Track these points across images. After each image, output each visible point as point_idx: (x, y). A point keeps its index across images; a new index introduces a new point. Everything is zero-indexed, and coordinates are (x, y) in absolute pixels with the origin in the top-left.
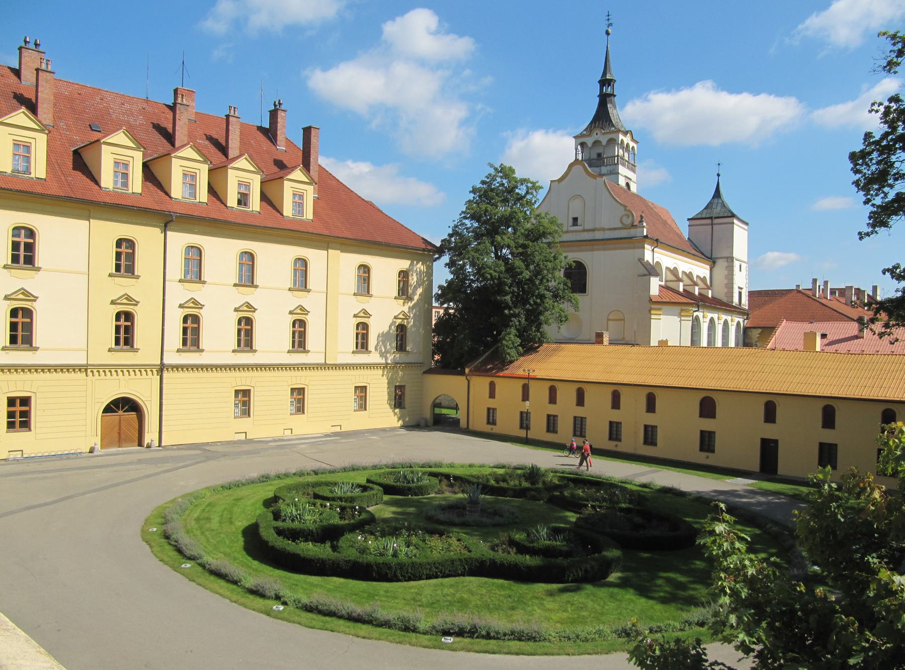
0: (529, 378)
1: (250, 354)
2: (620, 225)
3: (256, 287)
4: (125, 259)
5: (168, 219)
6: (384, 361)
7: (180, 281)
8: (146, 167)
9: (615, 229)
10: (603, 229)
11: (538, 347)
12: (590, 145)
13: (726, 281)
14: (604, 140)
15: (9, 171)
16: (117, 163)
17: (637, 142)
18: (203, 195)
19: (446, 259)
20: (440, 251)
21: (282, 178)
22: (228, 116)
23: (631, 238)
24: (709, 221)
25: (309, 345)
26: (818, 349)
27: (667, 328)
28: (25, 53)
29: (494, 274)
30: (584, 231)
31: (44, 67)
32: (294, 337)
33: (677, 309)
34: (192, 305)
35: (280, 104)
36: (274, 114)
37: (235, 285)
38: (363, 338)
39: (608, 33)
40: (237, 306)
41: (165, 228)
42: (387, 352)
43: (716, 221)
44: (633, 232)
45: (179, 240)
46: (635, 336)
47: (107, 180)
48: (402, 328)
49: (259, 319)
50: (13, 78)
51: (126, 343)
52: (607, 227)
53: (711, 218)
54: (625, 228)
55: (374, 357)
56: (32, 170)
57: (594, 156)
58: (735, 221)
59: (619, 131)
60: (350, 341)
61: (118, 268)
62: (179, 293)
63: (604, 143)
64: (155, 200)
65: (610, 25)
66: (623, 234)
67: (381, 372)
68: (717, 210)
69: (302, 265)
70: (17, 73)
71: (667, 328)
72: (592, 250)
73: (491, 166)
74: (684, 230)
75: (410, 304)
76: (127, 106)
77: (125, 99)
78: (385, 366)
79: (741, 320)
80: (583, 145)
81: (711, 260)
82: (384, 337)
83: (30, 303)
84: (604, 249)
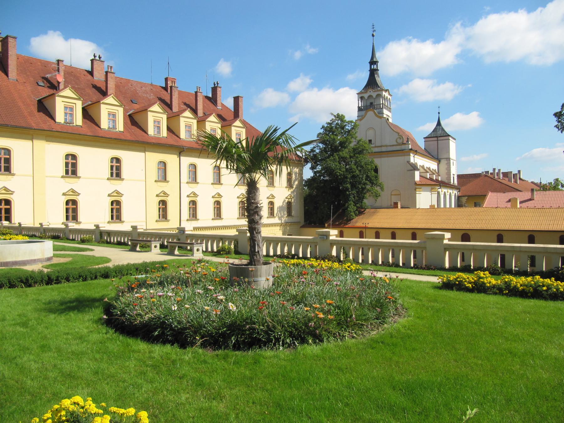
0: (366, 228)
1: (166, 223)
2: (396, 143)
3: (222, 184)
4: (72, 168)
5: (181, 150)
6: (280, 222)
7: (212, 184)
8: (84, 110)
9: (393, 146)
10: (387, 146)
11: (364, 211)
12: (366, 98)
13: (447, 171)
14: (374, 95)
15: (107, 128)
16: (66, 108)
17: (391, 95)
18: (164, 133)
19: (309, 165)
20: (306, 161)
21: (179, 115)
22: (196, 92)
23: (403, 150)
24: (436, 139)
25: (169, 216)
26: (518, 207)
27: (425, 199)
28: (95, 63)
29: (341, 172)
30: (376, 147)
31: (110, 70)
32: (159, 212)
33: (430, 188)
34: (116, 194)
35: (218, 84)
36: (214, 90)
37: (212, 184)
38: (163, 211)
39: (373, 36)
40: (65, 192)
41: (180, 155)
42: (282, 217)
43: (439, 138)
44: (403, 147)
45: (186, 161)
46: (410, 204)
47: (60, 117)
48: (289, 204)
49: (125, 202)
50: (89, 77)
51: (163, 217)
52: (389, 144)
53: (437, 137)
54: (399, 144)
55: (276, 220)
56: (117, 127)
57: (368, 104)
58: (450, 138)
59: (382, 90)
60: (211, 212)
61: (67, 172)
62: (187, 189)
63: (374, 96)
64: (172, 141)
65: (374, 31)
66: (398, 148)
67: (279, 228)
68: (440, 132)
69: (163, 166)
70: (91, 73)
71: (425, 199)
72: (381, 157)
73: (332, 114)
74: (421, 144)
75: (292, 190)
76: (143, 88)
77: (143, 85)
78: (281, 225)
79: (456, 192)
80: (362, 98)
81: (438, 160)
82: (280, 208)
83: (75, 197)
84: (388, 157)
